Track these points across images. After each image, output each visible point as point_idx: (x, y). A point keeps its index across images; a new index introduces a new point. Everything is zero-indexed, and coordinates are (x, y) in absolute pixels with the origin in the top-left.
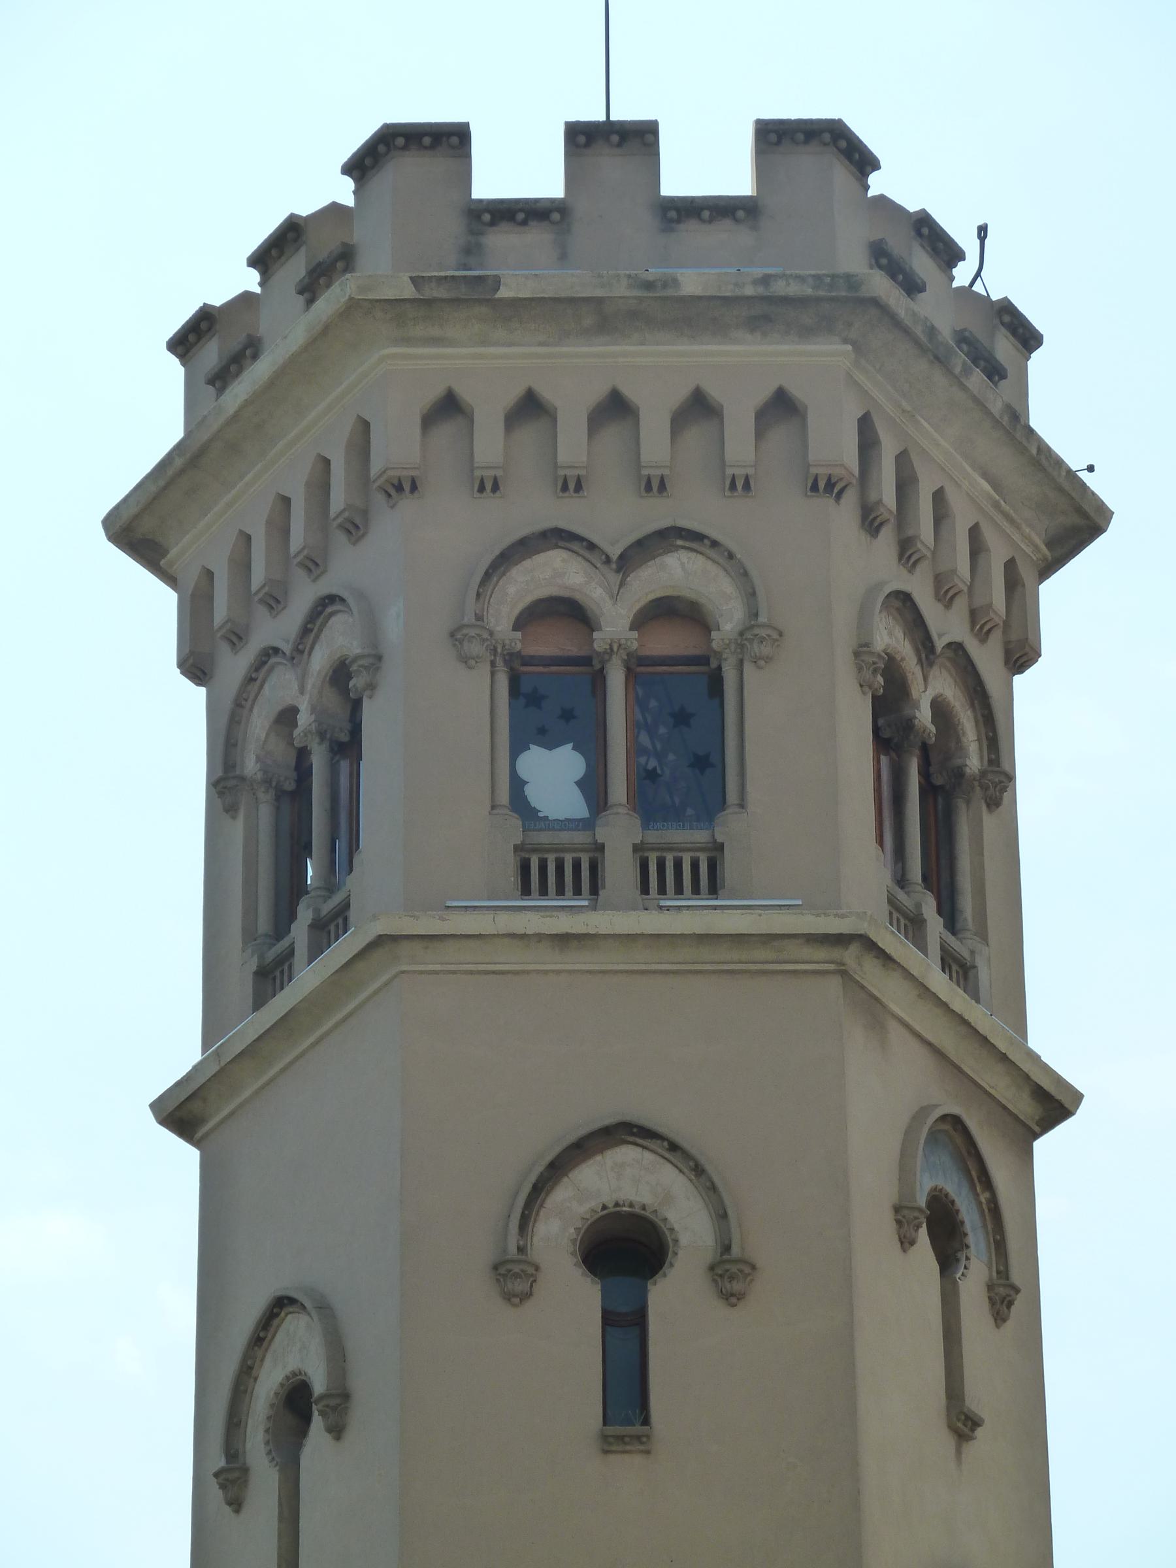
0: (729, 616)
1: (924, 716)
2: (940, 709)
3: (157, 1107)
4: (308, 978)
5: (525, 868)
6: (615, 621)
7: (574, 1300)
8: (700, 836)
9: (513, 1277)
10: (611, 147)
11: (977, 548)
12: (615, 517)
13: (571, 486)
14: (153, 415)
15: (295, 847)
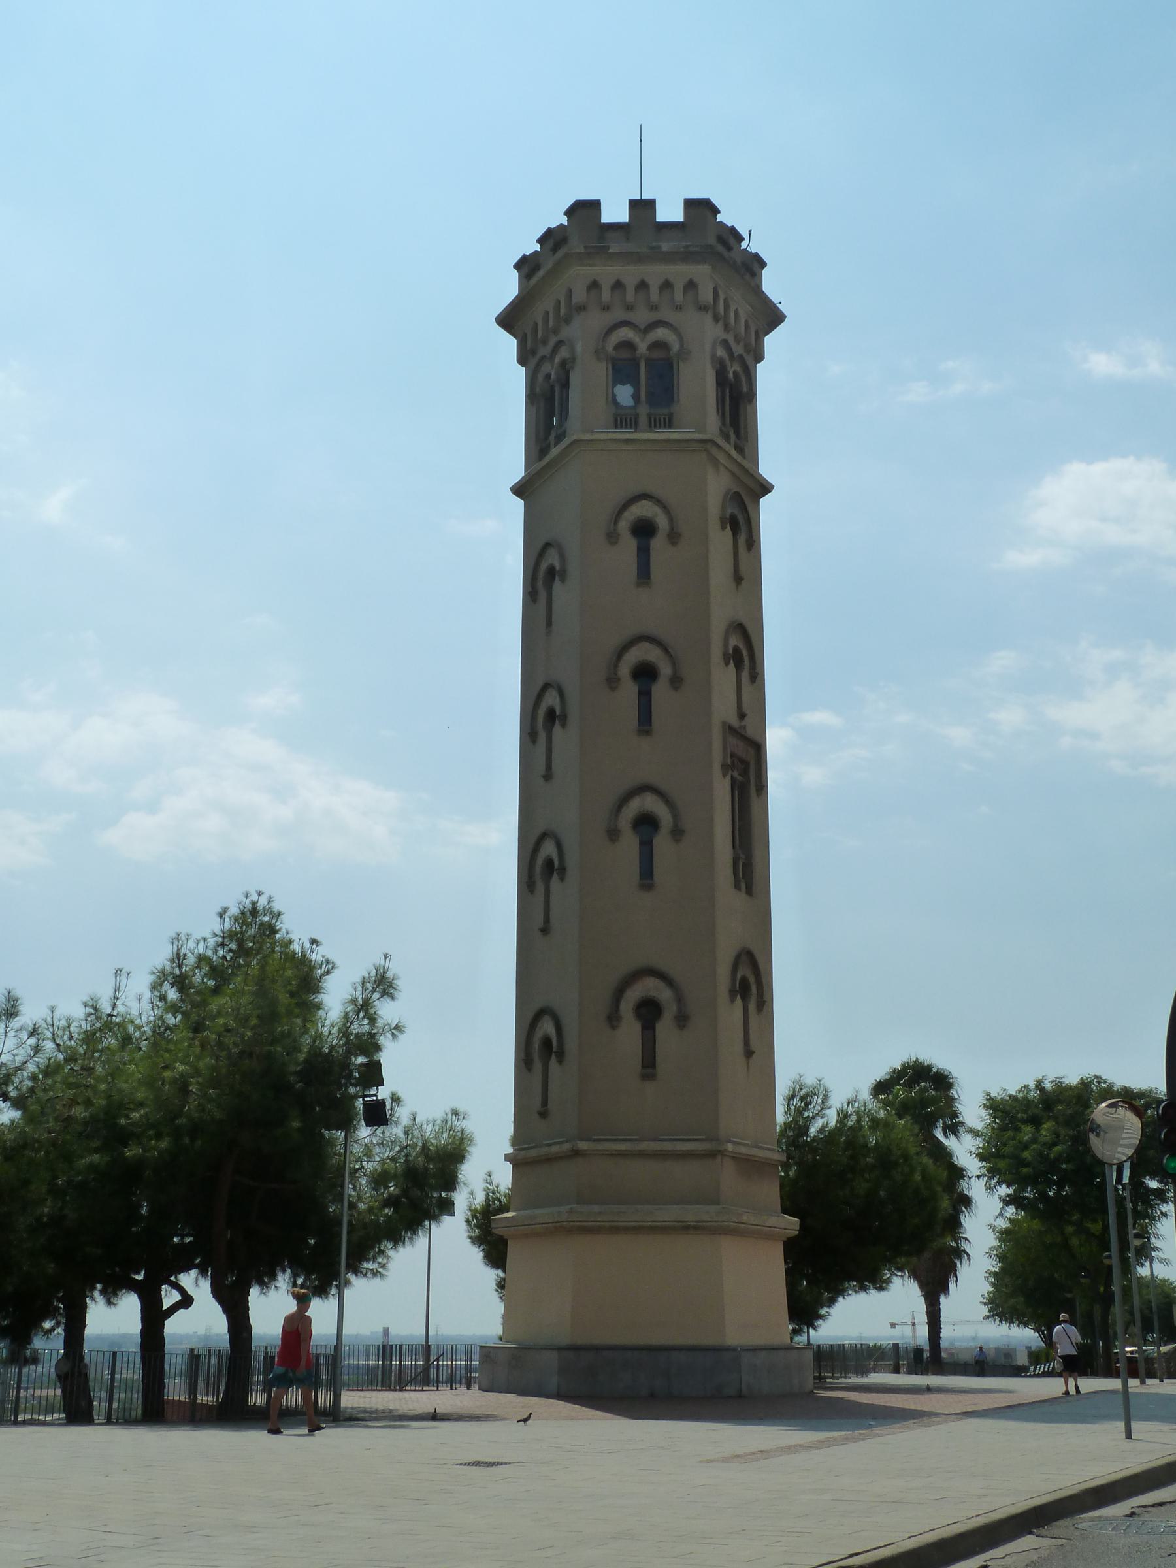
0: (676, 347)
1: (731, 375)
2: (735, 373)
3: (511, 489)
4: (555, 452)
5: (616, 421)
6: (643, 348)
7: (629, 544)
8: (665, 411)
9: (612, 682)
10: (642, 208)
11: (747, 326)
12: (642, 316)
13: (630, 308)
14: (509, 288)
15: (550, 414)
